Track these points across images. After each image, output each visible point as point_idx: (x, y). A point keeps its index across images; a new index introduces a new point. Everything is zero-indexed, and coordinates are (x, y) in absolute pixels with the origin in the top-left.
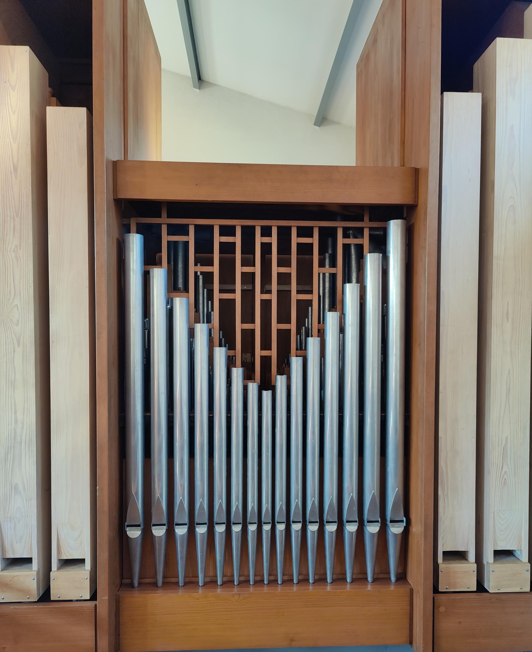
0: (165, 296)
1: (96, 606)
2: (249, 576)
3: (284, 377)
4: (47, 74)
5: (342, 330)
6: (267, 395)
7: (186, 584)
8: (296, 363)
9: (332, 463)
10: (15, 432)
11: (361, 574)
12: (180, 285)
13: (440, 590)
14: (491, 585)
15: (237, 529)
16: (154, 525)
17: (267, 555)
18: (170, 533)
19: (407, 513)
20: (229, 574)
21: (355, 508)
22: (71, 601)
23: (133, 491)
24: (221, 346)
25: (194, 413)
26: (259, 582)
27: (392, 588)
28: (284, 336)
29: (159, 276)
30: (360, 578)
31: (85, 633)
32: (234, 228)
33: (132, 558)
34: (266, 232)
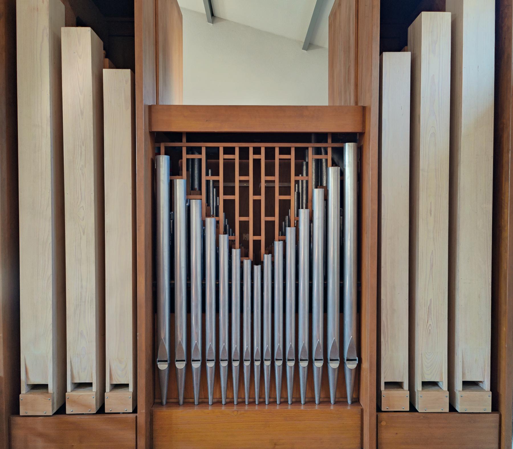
0: (185, 197)
1: (136, 417)
2: (245, 398)
3: (270, 255)
4: (102, 43)
5: (311, 221)
7: (200, 403)
8: (278, 246)
9: (304, 317)
10: (81, 295)
12: (196, 186)
13: (382, 410)
14: (419, 407)
15: (236, 364)
16: (177, 361)
17: (257, 383)
18: (189, 367)
20: (230, 397)
21: (321, 350)
22: (119, 413)
23: (162, 336)
24: (226, 234)
26: (252, 403)
27: (349, 408)
28: (270, 225)
29: (180, 184)
30: (325, 401)
31: (130, 435)
32: (234, 148)
33: (163, 383)
34: (257, 151)
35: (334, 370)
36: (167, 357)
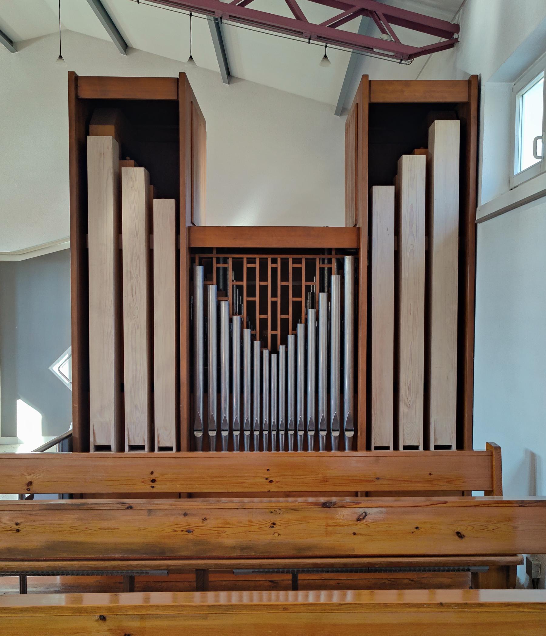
3: (284, 346)
6: (274, 356)
8: (291, 338)
28: (285, 322)
29: (212, 290)
34: (274, 261)
35: (335, 438)
36: (202, 428)
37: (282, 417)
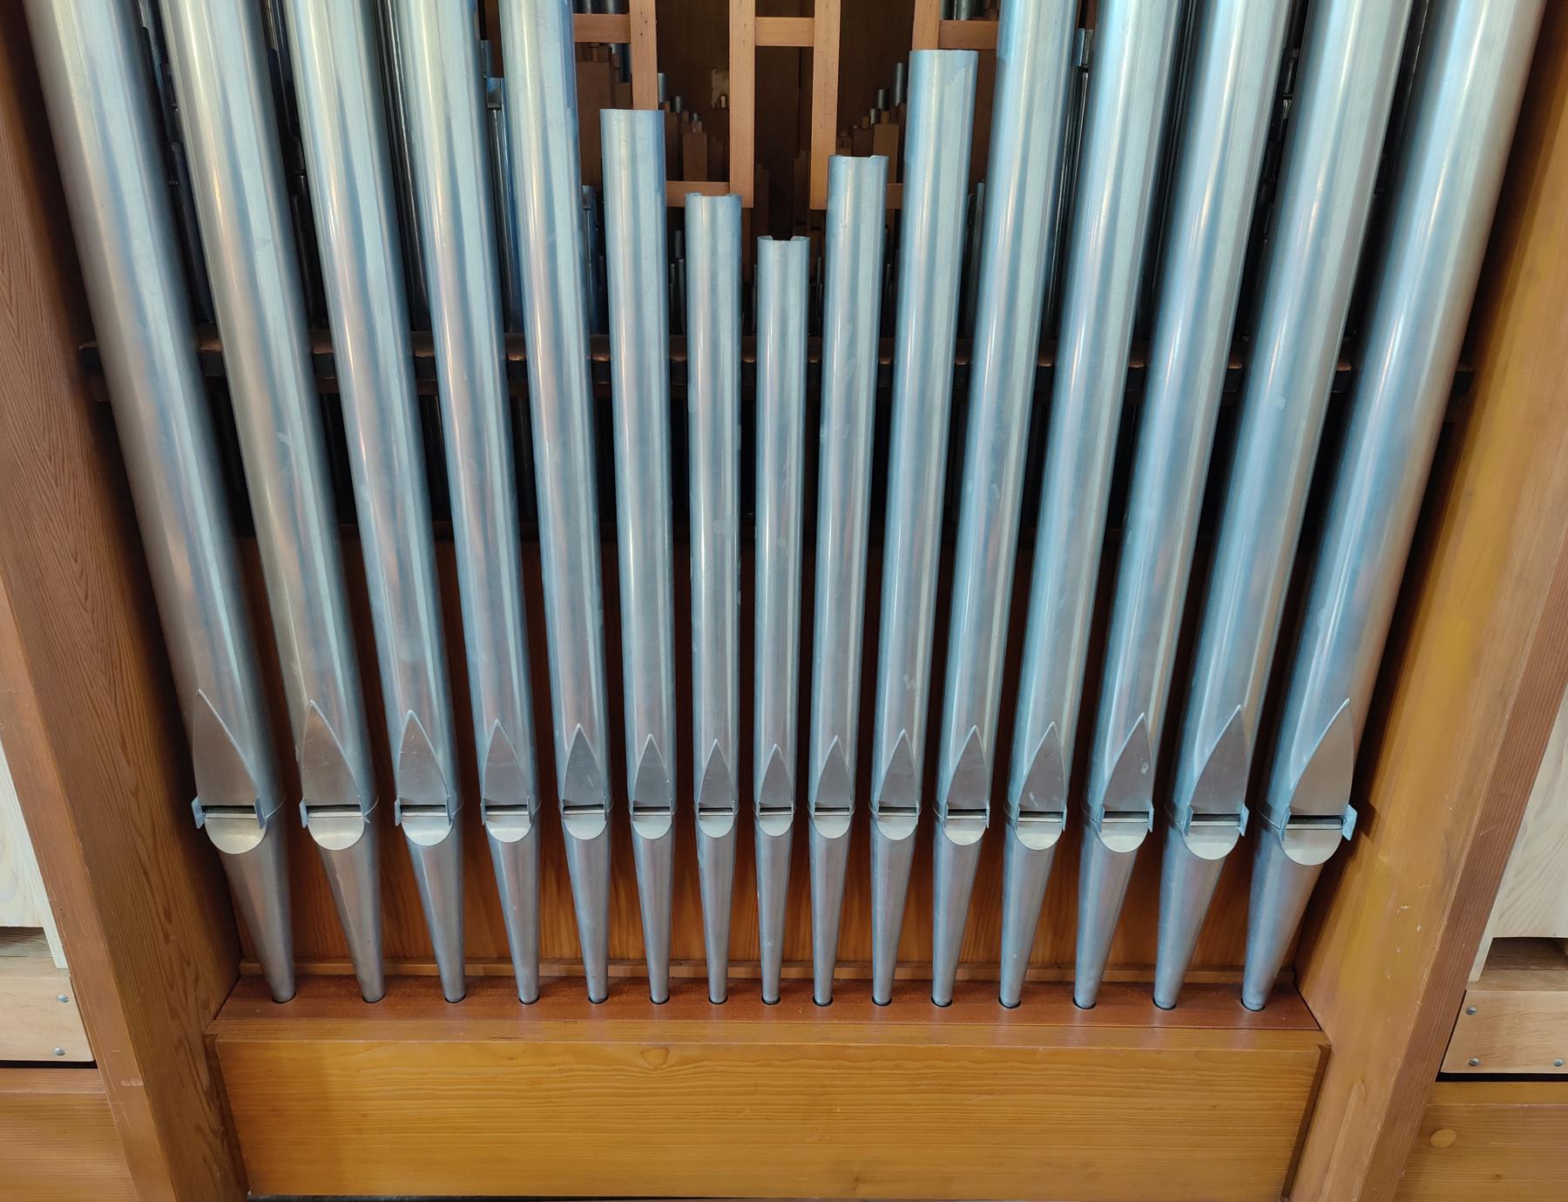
3: (874, 167)
6: (782, 260)
8: (937, 82)
11: (1126, 966)
19: (1361, 795)
25: (1039, 371)
33: (215, 943)
37: (837, 728)
